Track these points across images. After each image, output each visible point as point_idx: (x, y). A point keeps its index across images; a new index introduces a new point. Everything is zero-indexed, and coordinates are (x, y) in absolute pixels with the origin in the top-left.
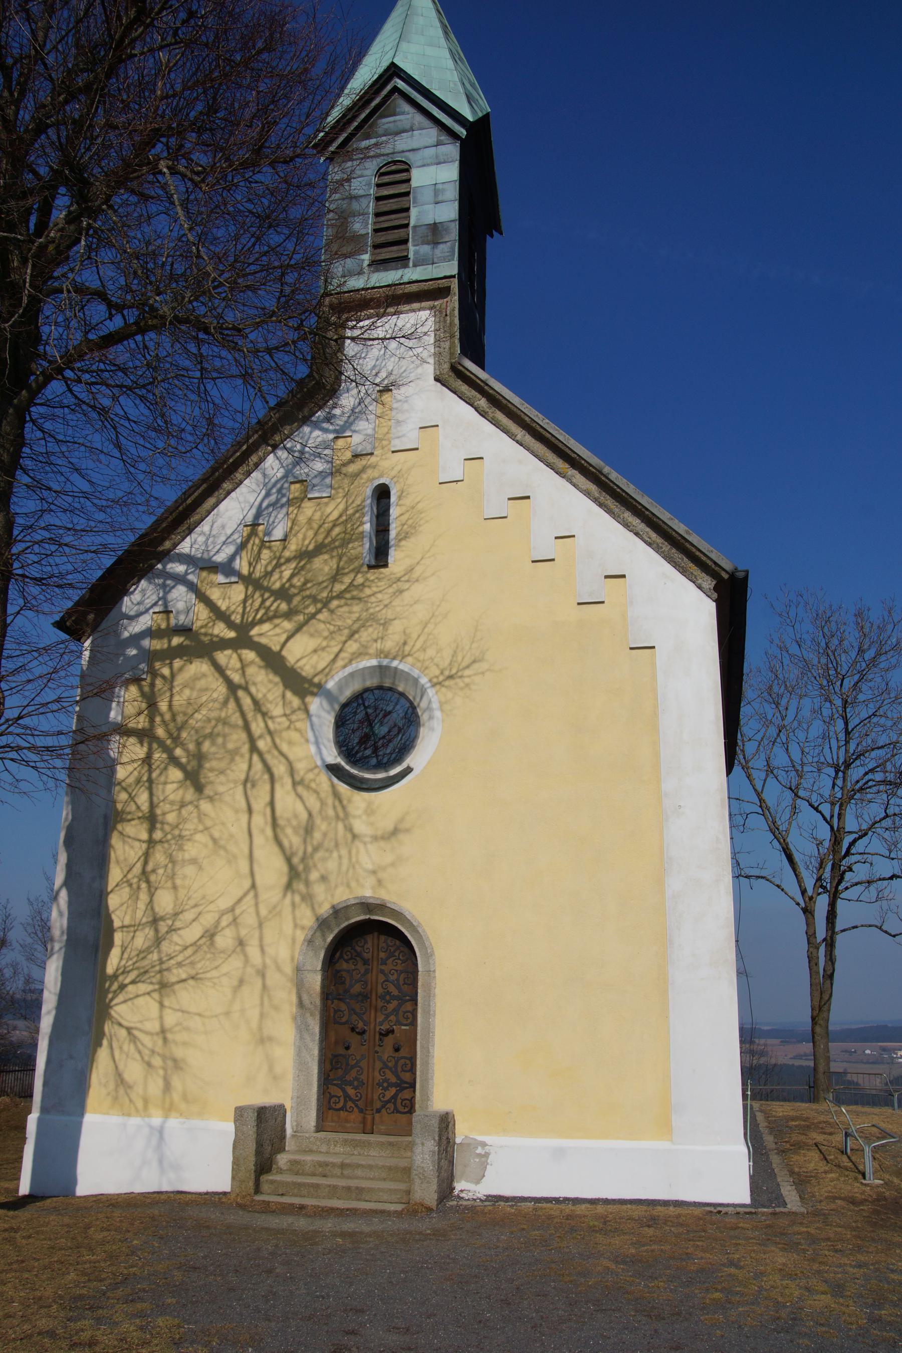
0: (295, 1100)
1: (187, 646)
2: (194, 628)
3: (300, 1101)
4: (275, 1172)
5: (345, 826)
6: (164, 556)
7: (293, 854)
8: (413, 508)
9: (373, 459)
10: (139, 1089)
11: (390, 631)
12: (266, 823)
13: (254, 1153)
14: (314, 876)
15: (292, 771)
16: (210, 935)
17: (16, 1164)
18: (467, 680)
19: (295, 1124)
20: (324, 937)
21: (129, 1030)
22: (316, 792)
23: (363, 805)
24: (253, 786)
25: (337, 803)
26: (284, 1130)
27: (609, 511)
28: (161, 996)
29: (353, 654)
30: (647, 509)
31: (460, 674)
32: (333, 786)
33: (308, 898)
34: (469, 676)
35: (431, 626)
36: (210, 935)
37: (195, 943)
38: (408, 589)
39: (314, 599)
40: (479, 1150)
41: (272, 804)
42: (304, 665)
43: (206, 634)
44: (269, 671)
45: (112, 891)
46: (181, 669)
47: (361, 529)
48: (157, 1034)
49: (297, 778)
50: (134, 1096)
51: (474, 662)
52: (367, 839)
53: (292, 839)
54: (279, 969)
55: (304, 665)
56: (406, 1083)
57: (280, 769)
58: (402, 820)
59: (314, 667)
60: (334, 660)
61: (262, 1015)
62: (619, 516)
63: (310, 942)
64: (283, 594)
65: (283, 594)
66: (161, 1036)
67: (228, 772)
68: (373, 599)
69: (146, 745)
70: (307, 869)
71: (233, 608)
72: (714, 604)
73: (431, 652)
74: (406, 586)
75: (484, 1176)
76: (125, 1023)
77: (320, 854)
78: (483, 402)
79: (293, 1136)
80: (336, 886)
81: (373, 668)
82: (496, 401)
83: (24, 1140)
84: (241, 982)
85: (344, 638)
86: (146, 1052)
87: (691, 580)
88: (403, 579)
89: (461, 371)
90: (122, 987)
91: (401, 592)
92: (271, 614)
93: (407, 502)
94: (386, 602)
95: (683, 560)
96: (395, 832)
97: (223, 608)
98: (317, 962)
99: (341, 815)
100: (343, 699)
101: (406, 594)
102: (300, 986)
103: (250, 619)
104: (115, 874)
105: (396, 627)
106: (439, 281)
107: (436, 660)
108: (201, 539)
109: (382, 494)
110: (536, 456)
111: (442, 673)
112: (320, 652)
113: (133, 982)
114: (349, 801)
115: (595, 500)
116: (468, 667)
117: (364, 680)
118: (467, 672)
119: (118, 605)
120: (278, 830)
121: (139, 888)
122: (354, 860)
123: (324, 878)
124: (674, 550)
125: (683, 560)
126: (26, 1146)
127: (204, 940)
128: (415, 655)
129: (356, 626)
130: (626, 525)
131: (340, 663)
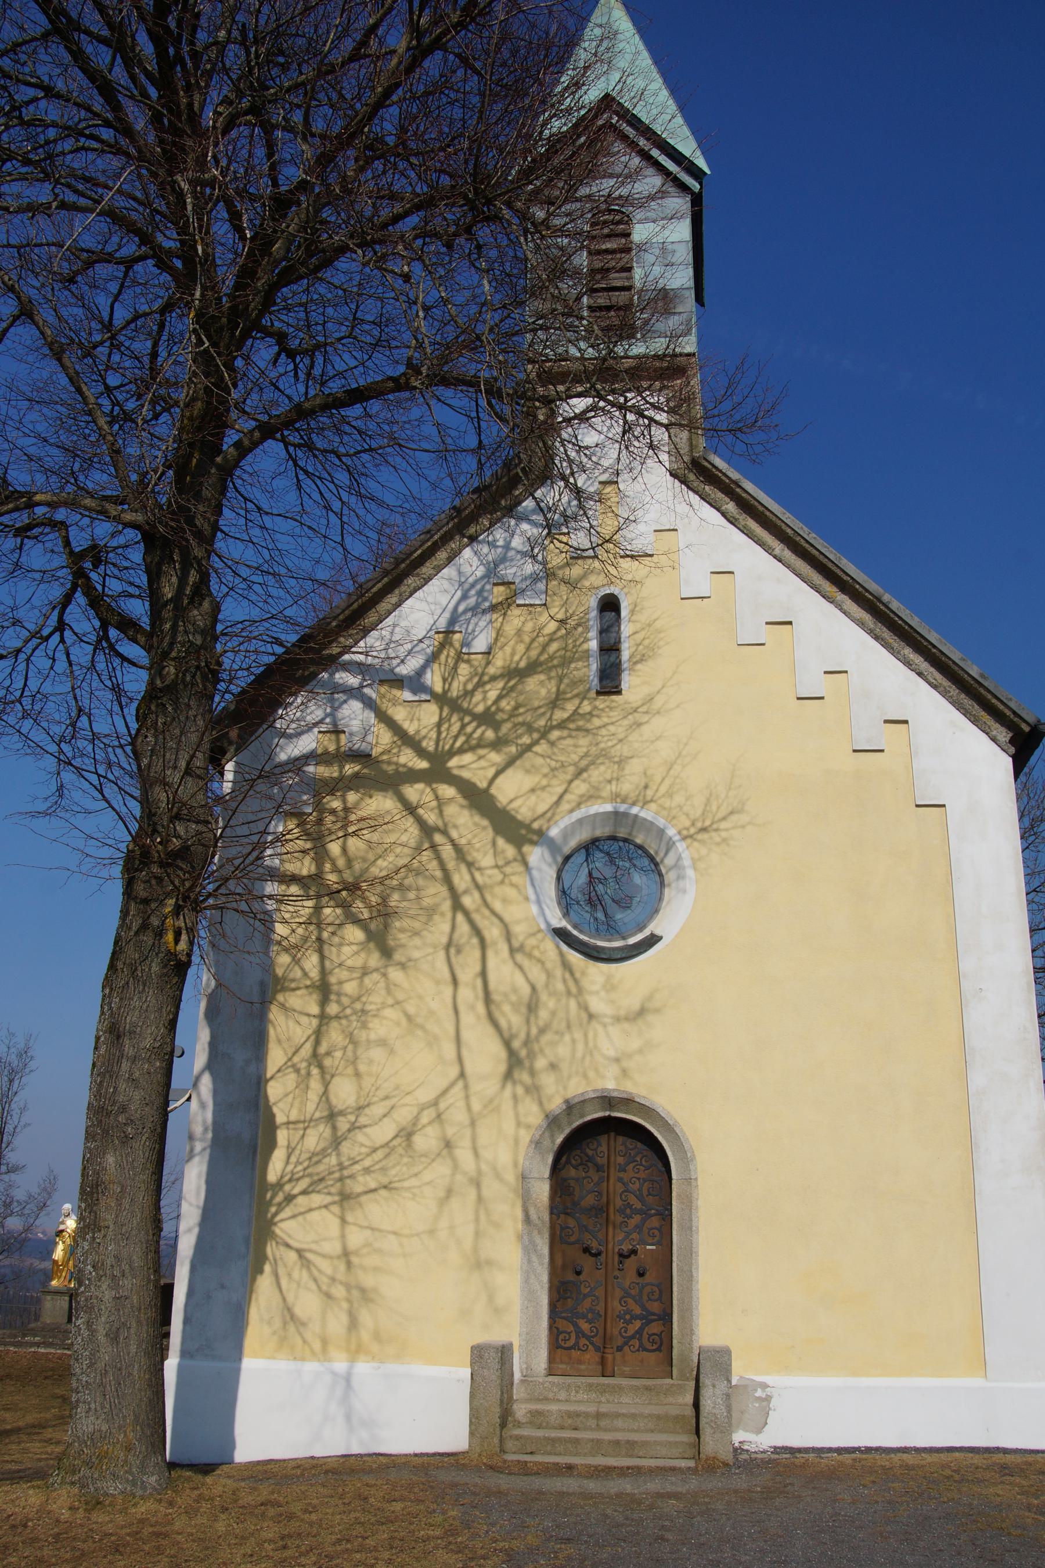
3: (529, 1339)
6: (332, 662)
25: (567, 976)
33: (534, 1090)
38: (647, 722)
40: (759, 1393)
41: (483, 974)
48: (339, 1257)
50: (309, 1336)
54: (498, 1177)
55: (520, 807)
58: (650, 997)
62: (899, 652)
63: (537, 1144)
71: (423, 732)
73: (678, 799)
78: (731, 507)
79: (522, 1381)
80: (570, 1077)
82: (748, 507)
86: (324, 1280)
87: (983, 731)
89: (706, 468)
92: (474, 742)
93: (643, 617)
96: (642, 1012)
102: (526, 1198)
103: (447, 747)
120: (493, 1007)
127: (399, 1140)
129: (583, 763)
130: (908, 663)
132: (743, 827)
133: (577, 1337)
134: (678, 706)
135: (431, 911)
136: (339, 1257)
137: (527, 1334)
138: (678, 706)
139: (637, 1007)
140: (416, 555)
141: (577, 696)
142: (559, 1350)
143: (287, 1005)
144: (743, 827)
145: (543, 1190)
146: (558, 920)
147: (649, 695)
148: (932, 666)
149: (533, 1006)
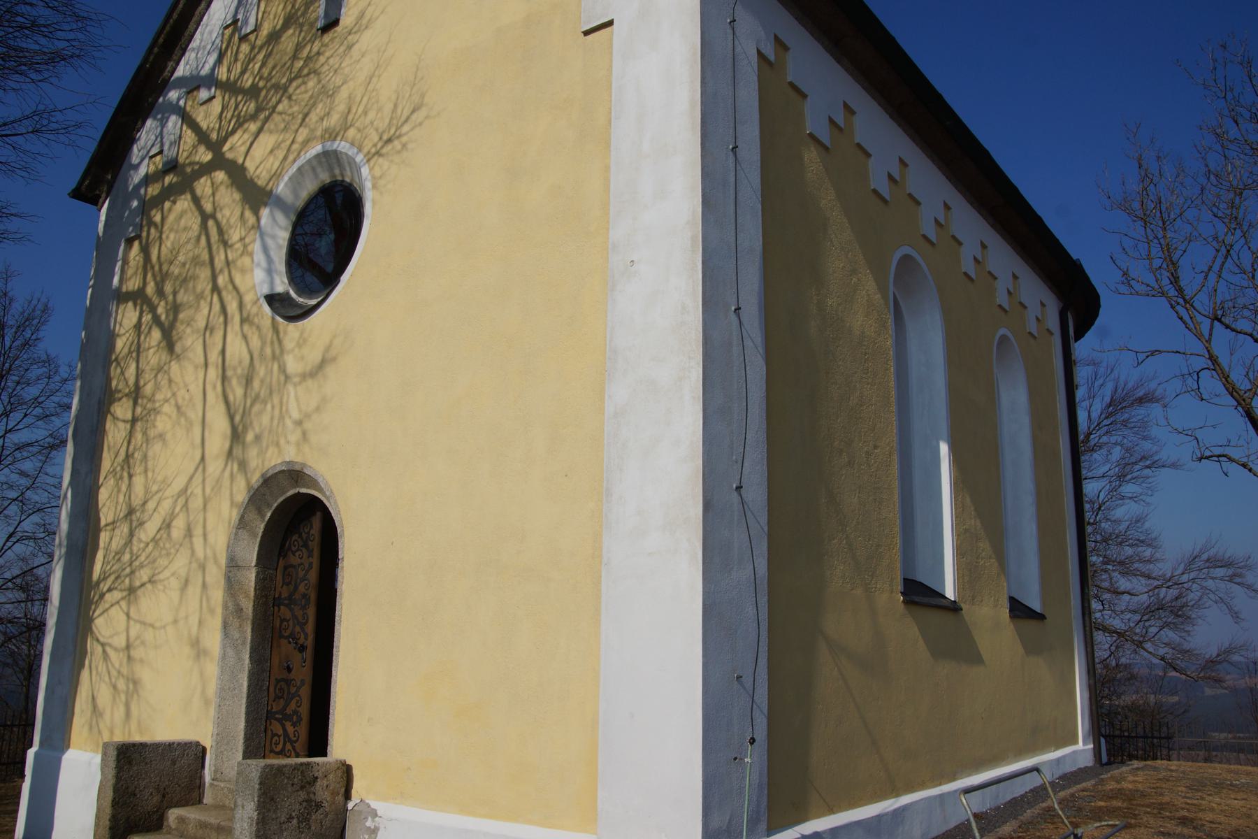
0: (214, 737)
2: (181, 160)
3: (222, 737)
4: (164, 831)
5: (280, 367)
6: (164, 86)
7: (236, 412)
10: (107, 717)
11: (336, 103)
13: (110, 805)
14: (250, 437)
15: (241, 306)
16: (167, 525)
17: (17, 800)
18: (404, 139)
20: (261, 513)
21: (103, 645)
22: (258, 328)
24: (211, 333)
26: (201, 777)
28: (129, 604)
29: (303, 142)
31: (398, 133)
32: (273, 319)
33: (243, 465)
35: (375, 80)
36: (167, 525)
38: (357, 41)
39: (276, 87)
40: (369, 823)
41: (223, 352)
45: (102, 484)
46: (170, 210)
48: (123, 650)
49: (245, 315)
50: (102, 726)
51: (413, 111)
52: (296, 380)
53: (237, 391)
57: (232, 307)
58: (328, 348)
59: (269, 171)
60: (285, 158)
63: (242, 523)
64: (253, 92)
65: (253, 92)
66: (126, 652)
67: (192, 323)
68: (326, 67)
69: (138, 308)
73: (371, 115)
74: (355, 37)
76: (102, 639)
79: (211, 785)
80: (267, 448)
81: (317, 156)
83: (23, 776)
84: (187, 582)
85: (296, 126)
86: (114, 673)
88: (354, 31)
90: (102, 596)
91: (350, 47)
92: (242, 120)
94: (336, 66)
96: (323, 363)
98: (250, 553)
101: (356, 47)
102: (231, 585)
103: (224, 134)
104: (106, 464)
105: (344, 93)
108: (193, 55)
113: (110, 590)
114: (285, 333)
117: (316, 175)
118: (405, 129)
119: (127, 159)
121: (121, 478)
123: (258, 438)
126: (24, 784)
129: (306, 110)
131: (291, 158)
133: (285, 743)
134: (382, 12)
135: (200, 297)
136: (123, 650)
137: (218, 734)
138: (382, 12)
142: (272, 754)
143: (115, 416)
144: (420, 124)
145: (250, 578)
146: (281, 285)
149: (249, 378)
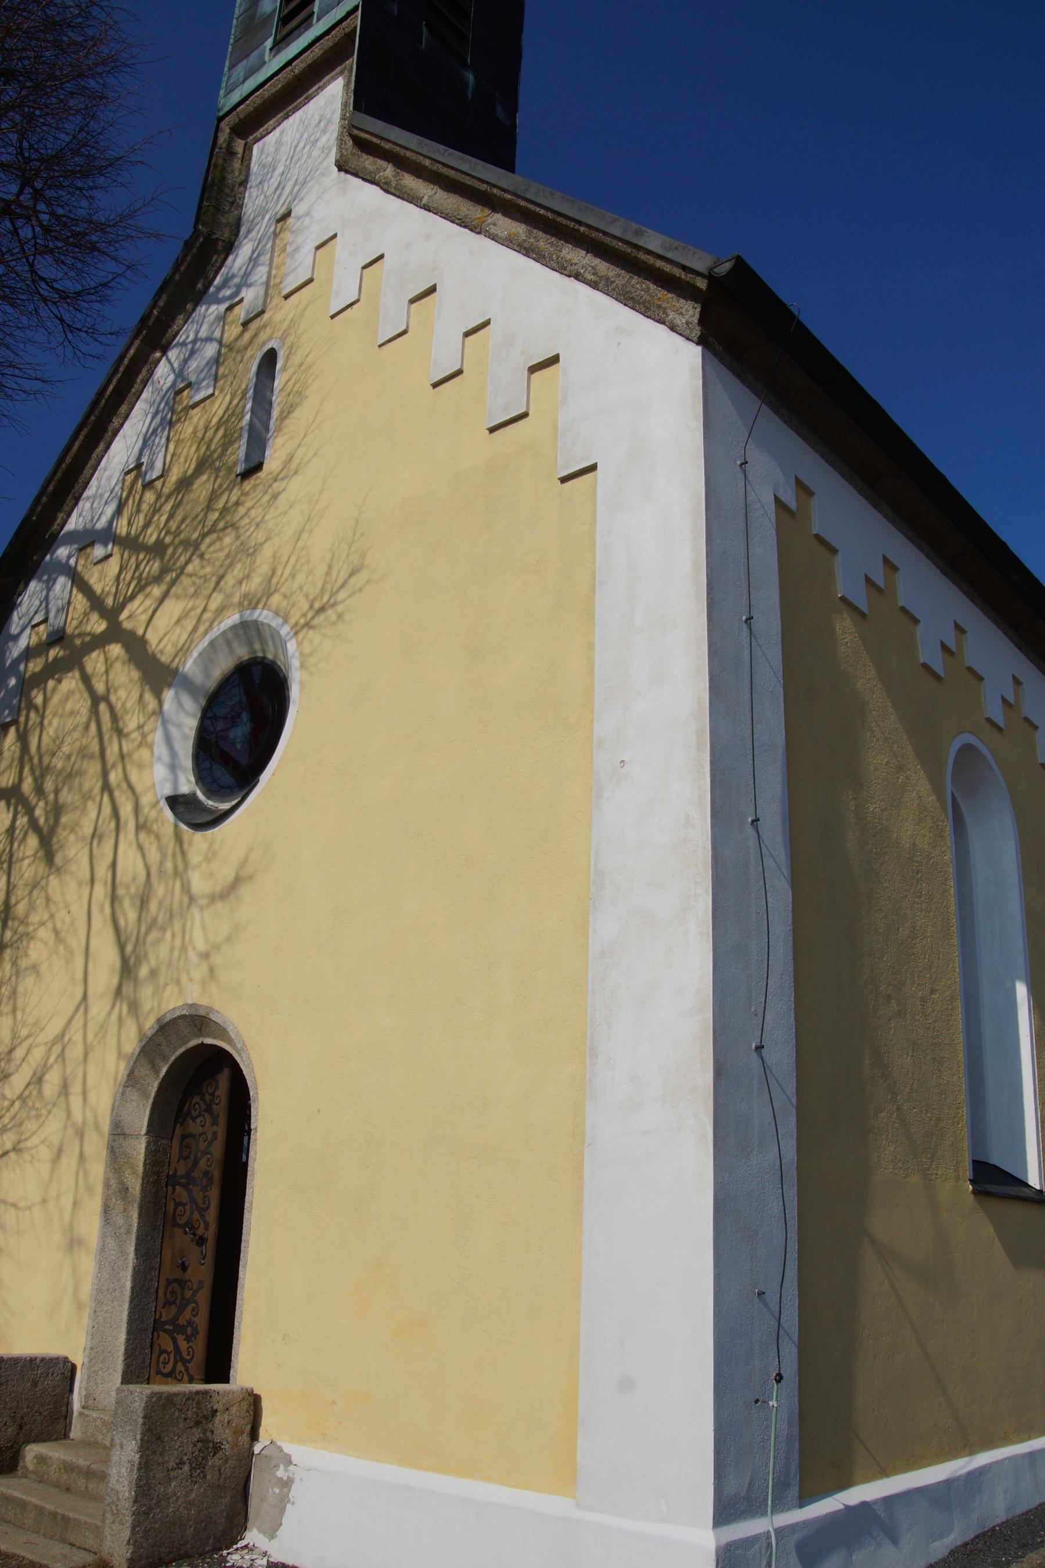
0: (87, 1351)
1: (62, 658)
2: (69, 630)
3: (97, 1353)
5: (183, 886)
6: (51, 542)
8: (301, 364)
9: (266, 316)
12: (106, 896)
15: (137, 809)
16: (38, 1080)
18: (340, 608)
19: (84, 1393)
22: (158, 837)
23: (204, 846)
24: (100, 841)
25: (178, 848)
26: (69, 1404)
27: (539, 257)
29: (217, 610)
30: (580, 223)
31: (332, 601)
32: (176, 826)
33: (134, 1007)
34: (343, 601)
36: (38, 1080)
37: (21, 1095)
40: (281, 1473)
41: (114, 865)
42: (165, 647)
43: (80, 635)
44: (132, 667)
46: (54, 690)
47: (240, 425)
49: (141, 820)
52: (203, 902)
53: (129, 915)
54: (97, 1127)
55: (165, 647)
56: (166, 1331)
57: (126, 810)
60: (195, 629)
61: (75, 1204)
62: (551, 259)
63: (132, 1079)
67: (77, 828)
69: (12, 809)
70: (138, 962)
71: (107, 589)
72: (698, 350)
73: (300, 578)
75: (281, 1524)
77: (153, 936)
78: (389, 171)
79: (81, 1414)
80: (166, 985)
82: (402, 163)
87: (658, 321)
89: (365, 140)
91: (275, 496)
92: (143, 582)
93: (296, 360)
95: (648, 290)
96: (236, 882)
97: (98, 591)
99: (181, 867)
100: (212, 684)
102: (115, 1157)
106: (344, 24)
107: (305, 588)
108: (88, 505)
109: (270, 359)
110: (446, 217)
111: (311, 607)
112: (183, 622)
114: (191, 843)
115: (527, 251)
116: (342, 586)
117: (231, 650)
118: (342, 595)
120: (116, 905)
122: (187, 938)
123: (153, 973)
124: (635, 280)
125: (648, 290)
127: (31, 1087)
128: (283, 590)
129: (221, 572)
130: (562, 268)
131: (202, 629)
132: (360, 590)
133: (176, 1362)
135: (86, 797)
137: (91, 1349)
138: (315, 454)
139: (231, 877)
140: (108, 393)
141: (225, 490)
144: (360, 590)
147: (290, 453)
148: (596, 255)
